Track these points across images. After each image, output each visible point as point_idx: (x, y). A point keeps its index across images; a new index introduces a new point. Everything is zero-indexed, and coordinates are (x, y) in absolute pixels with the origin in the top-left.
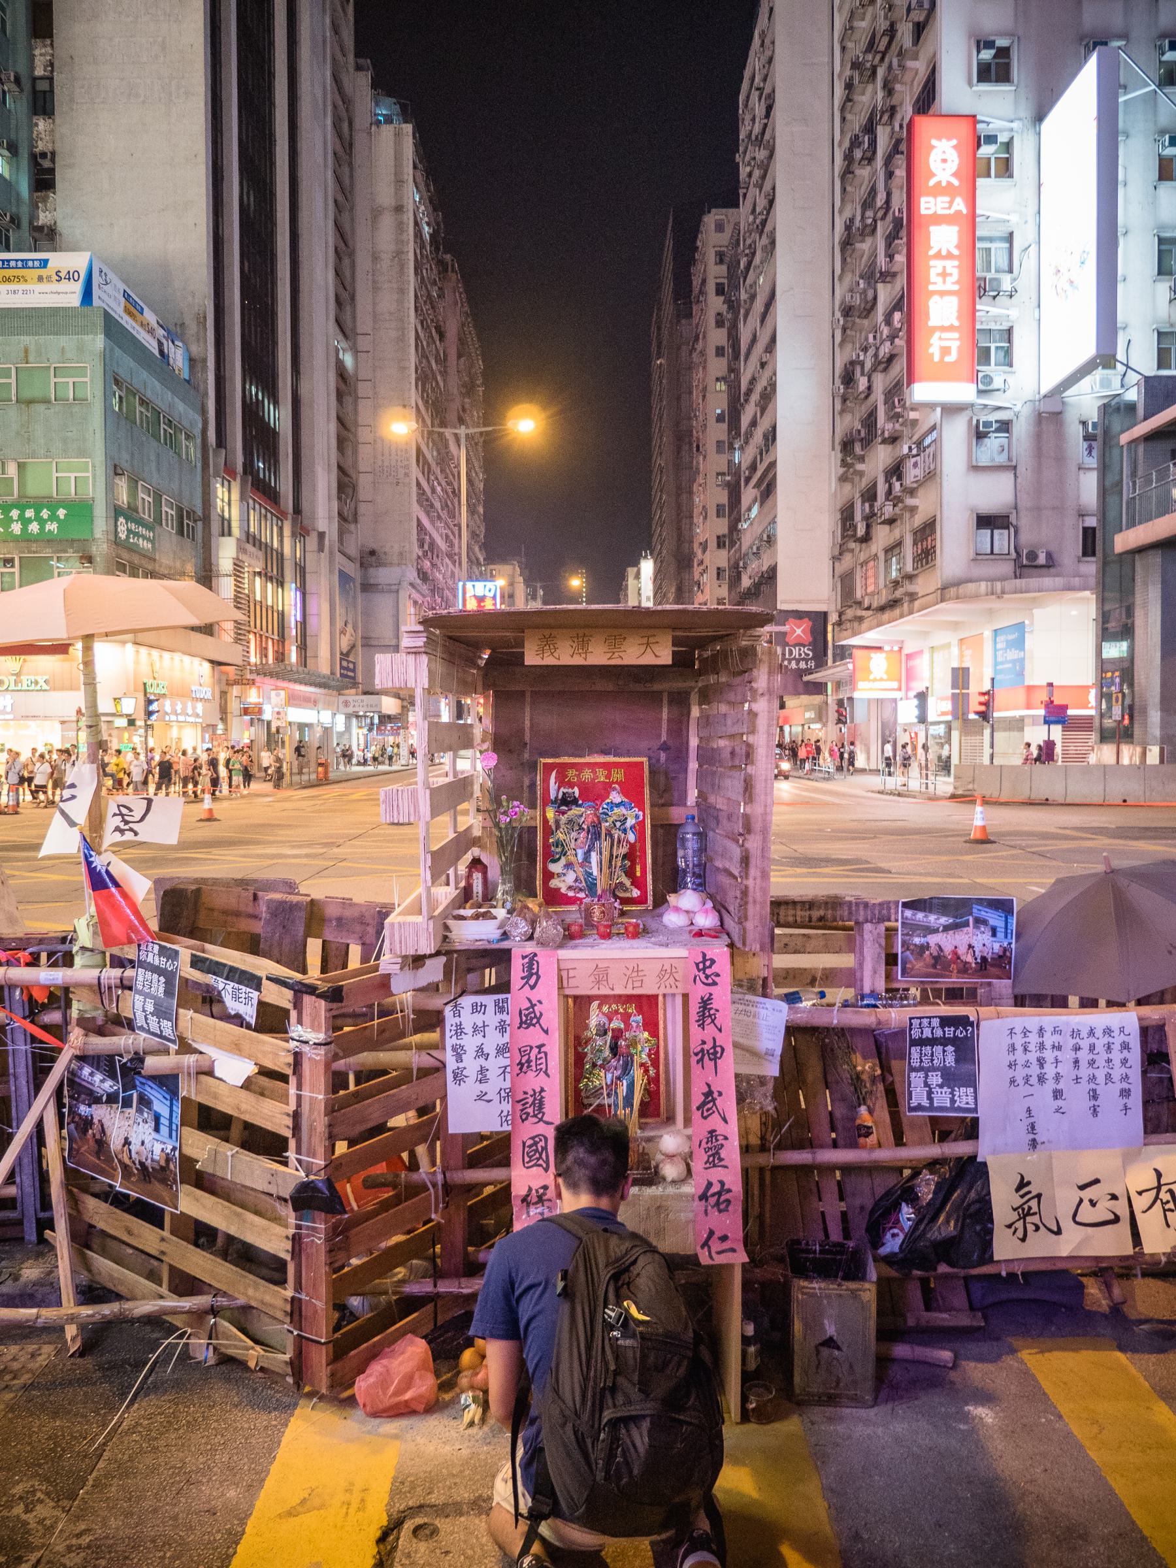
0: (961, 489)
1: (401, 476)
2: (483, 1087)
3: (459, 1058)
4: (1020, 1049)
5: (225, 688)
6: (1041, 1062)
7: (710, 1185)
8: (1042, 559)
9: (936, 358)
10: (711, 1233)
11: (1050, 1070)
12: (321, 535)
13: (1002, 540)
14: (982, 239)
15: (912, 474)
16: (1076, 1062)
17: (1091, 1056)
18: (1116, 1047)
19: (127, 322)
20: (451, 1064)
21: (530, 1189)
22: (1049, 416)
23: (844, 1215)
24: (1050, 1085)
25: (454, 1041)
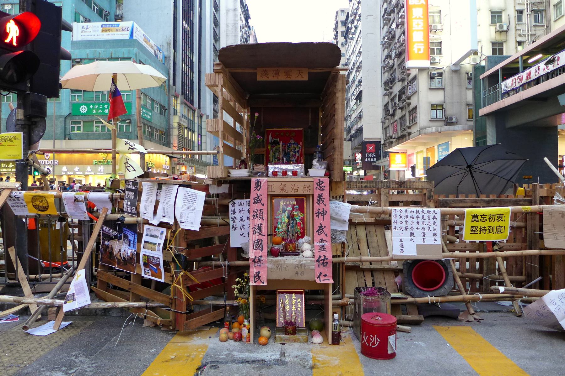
0: (424, 96)
2: (243, 231)
3: (234, 222)
5: (174, 166)
6: (406, 222)
7: (320, 257)
8: (454, 120)
9: (416, 52)
10: (321, 274)
11: (409, 225)
12: (208, 116)
13: (440, 114)
14: (431, 12)
15: (409, 92)
16: (418, 222)
17: (423, 220)
18: (432, 217)
19: (144, 44)
21: (256, 257)
22: (456, 70)
24: (409, 231)
25: (232, 215)
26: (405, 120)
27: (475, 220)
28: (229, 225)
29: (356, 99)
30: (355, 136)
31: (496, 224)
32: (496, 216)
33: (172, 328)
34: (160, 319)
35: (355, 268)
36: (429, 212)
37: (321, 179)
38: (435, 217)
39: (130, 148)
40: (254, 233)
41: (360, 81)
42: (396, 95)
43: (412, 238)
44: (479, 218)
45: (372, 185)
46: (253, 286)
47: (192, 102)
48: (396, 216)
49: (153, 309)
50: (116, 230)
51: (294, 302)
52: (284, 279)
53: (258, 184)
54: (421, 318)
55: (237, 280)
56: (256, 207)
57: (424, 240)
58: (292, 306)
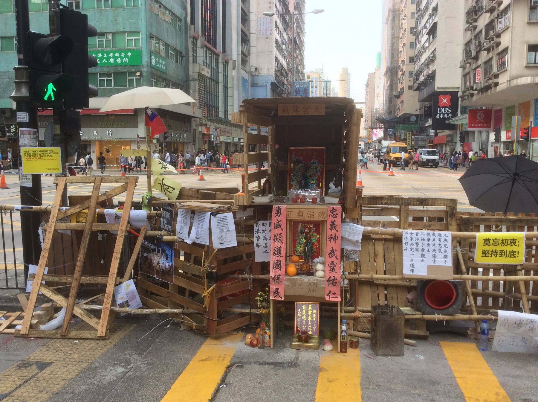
1: (268, 34)
2: (266, 249)
3: (258, 240)
4: (409, 239)
6: (417, 244)
10: (330, 292)
11: (420, 247)
15: (499, 27)
16: (429, 244)
17: (434, 243)
18: (442, 240)
20: (256, 242)
23: (97, 330)
24: (420, 252)
25: (257, 235)
26: (491, 66)
27: (487, 244)
28: (254, 243)
29: (429, 33)
30: (424, 84)
31: (509, 248)
32: (509, 241)
33: (205, 333)
34: (195, 324)
35: (370, 283)
36: (439, 235)
37: (335, 207)
38: (446, 240)
39: (162, 167)
40: (274, 254)
41: (435, 9)
42: (481, 31)
43: (423, 258)
44: (491, 242)
45: (392, 202)
46: (273, 300)
47: (215, 45)
48: (407, 238)
49: (188, 315)
50: (154, 244)
51: (310, 313)
52: (299, 295)
53: (279, 210)
54: (428, 334)
55: (259, 294)
56: (277, 231)
57: (434, 261)
58: (307, 316)
